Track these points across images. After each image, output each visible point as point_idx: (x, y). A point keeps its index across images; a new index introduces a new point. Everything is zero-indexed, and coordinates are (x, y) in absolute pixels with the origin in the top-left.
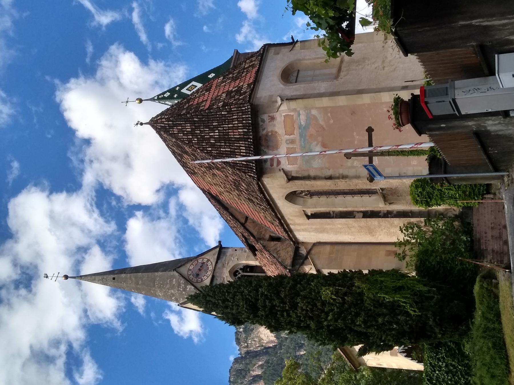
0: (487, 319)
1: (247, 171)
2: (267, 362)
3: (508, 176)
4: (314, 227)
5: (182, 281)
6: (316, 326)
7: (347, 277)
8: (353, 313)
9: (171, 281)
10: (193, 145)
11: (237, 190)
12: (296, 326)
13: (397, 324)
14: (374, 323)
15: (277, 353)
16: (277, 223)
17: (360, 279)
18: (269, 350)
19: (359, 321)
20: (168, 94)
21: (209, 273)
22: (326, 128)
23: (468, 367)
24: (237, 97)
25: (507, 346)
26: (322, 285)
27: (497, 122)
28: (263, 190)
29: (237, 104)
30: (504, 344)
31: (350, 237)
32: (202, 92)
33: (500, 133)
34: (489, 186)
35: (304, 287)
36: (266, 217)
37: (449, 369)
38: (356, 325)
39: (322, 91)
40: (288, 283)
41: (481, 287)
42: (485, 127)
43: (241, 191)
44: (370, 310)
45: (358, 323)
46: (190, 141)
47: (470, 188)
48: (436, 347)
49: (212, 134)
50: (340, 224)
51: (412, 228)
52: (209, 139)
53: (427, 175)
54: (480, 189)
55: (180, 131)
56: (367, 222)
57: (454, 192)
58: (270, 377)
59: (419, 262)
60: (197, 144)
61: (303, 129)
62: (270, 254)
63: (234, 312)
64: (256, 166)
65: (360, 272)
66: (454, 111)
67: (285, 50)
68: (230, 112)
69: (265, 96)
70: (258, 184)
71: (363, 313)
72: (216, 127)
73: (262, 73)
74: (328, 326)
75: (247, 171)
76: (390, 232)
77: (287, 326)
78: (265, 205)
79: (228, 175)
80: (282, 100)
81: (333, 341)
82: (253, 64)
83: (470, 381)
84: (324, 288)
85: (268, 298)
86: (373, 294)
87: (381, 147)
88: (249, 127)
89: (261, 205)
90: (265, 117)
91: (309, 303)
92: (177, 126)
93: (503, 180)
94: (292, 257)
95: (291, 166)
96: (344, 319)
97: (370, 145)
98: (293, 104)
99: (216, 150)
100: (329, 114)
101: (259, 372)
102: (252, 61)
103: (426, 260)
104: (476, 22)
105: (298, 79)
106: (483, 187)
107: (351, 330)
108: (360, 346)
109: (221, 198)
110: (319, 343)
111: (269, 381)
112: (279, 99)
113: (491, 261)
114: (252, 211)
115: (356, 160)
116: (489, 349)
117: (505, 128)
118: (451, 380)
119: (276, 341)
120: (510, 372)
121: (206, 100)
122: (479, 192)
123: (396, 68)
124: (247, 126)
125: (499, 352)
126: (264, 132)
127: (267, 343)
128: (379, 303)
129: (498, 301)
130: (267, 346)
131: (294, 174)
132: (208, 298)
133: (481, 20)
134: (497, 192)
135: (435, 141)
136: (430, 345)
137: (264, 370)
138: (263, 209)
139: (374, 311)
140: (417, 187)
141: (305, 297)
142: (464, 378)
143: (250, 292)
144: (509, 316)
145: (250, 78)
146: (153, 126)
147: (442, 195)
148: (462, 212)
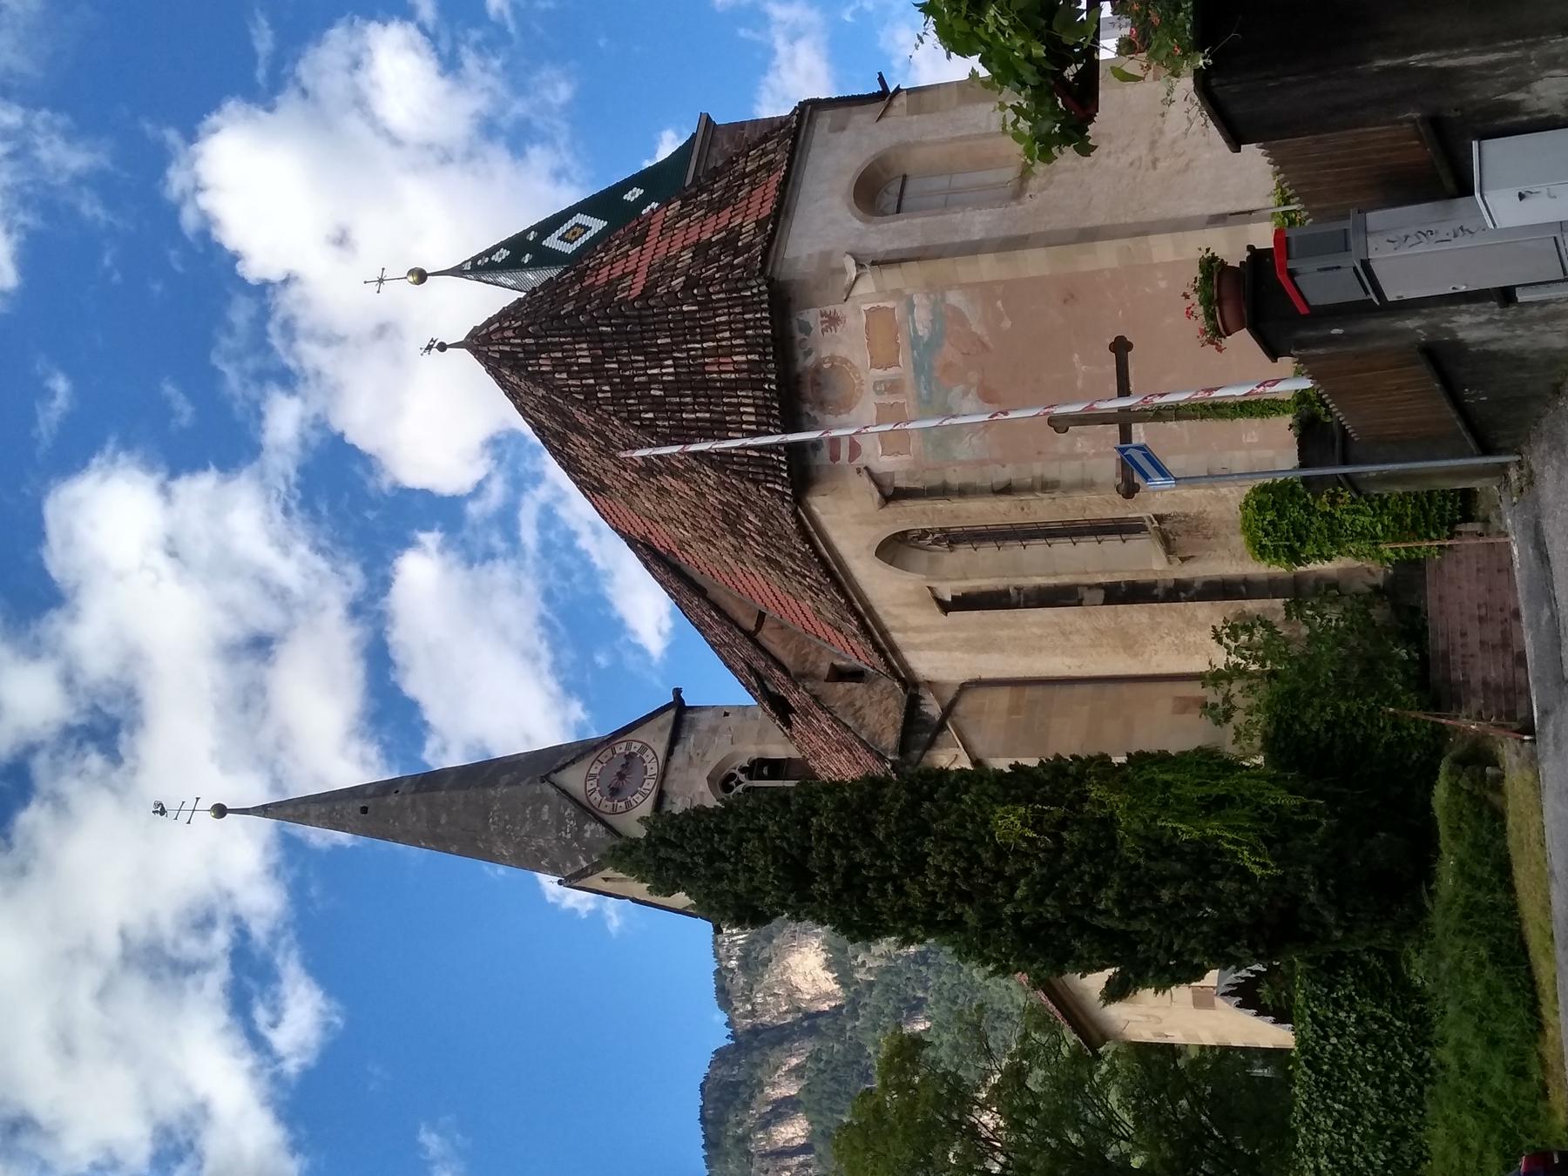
0: (1472, 878)
1: (762, 477)
2: (815, 1057)
3: (1520, 464)
4: (962, 635)
5: (570, 811)
6: (980, 920)
7: (1066, 775)
8: (1087, 878)
9: (536, 812)
10: (599, 406)
11: (733, 534)
12: (922, 922)
13: (1215, 903)
14: (1148, 904)
15: (843, 1030)
16: (853, 626)
17: (1102, 779)
18: (821, 1021)
19: (1105, 899)
20: (505, 253)
21: (650, 784)
22: (991, 345)
23: (1422, 1021)
24: (725, 260)
25: (1531, 953)
26: (994, 800)
27: (1482, 318)
28: (809, 532)
29: (725, 280)
30: (1524, 948)
31: (1068, 661)
32: (619, 247)
33: (1493, 347)
34: (1468, 496)
35: (940, 809)
36: (819, 611)
37: (1366, 1030)
38: (1095, 912)
39: (977, 234)
40: (896, 798)
41: (1455, 789)
42: (1451, 332)
43: (744, 537)
44: (1137, 866)
45: (1102, 907)
46: (590, 393)
47: (1414, 506)
48: (1328, 969)
49: (655, 371)
50: (1035, 624)
51: (1249, 630)
52: (646, 387)
53: (1294, 469)
54: (1443, 508)
55: (558, 365)
56: (1117, 616)
57: (1367, 520)
58: (826, 1103)
59: (1274, 724)
60: (613, 401)
61: (925, 350)
62: (836, 720)
63: (741, 887)
64: (789, 462)
65: (1104, 760)
66: (1367, 292)
67: (862, 118)
68: (706, 304)
69: (810, 256)
70: (795, 514)
71: (1116, 877)
72: (667, 351)
73: (797, 185)
74: (1017, 917)
75: (762, 477)
76: (1188, 643)
77: (895, 921)
78: (815, 574)
79: (705, 489)
80: (859, 265)
81: (1032, 961)
82: (771, 162)
83: (1428, 1061)
84: (1000, 810)
85: (837, 845)
86: (1143, 820)
87: (1162, 395)
88: (765, 346)
89: (804, 577)
90: (812, 317)
91: (957, 853)
92: (550, 351)
93: (1506, 476)
94: (899, 726)
95: (892, 459)
96: (1062, 896)
97: (1124, 391)
98: (893, 278)
99: (669, 419)
100: (999, 303)
101: (789, 1089)
102: (765, 153)
103: (1294, 718)
104: (1421, 61)
105: (905, 203)
106: (1453, 502)
107: (1083, 928)
108: (1110, 972)
109: (682, 558)
110: (990, 968)
111: (820, 1113)
112: (850, 264)
113: (1480, 713)
114: (778, 593)
115: (1080, 434)
116: (1480, 964)
117: (1507, 334)
118: (1373, 1061)
119: (840, 994)
120: (1541, 1027)
121: (634, 272)
122: (1442, 517)
123: (1191, 160)
124: (759, 345)
125: (1510, 972)
126: (810, 361)
127: (811, 1000)
128: (1161, 847)
129: (1504, 827)
130: (814, 1010)
131: (901, 483)
132: (662, 853)
133: (1433, 55)
134: (1493, 514)
135: (1314, 377)
136: (1309, 961)
137: (805, 1082)
138: (810, 587)
139: (1148, 869)
140: (1261, 508)
141: (946, 837)
142: (1411, 1053)
143: (785, 829)
144: (1534, 869)
145: (761, 203)
146: (477, 353)
147: (1336, 528)
148: (1395, 576)
